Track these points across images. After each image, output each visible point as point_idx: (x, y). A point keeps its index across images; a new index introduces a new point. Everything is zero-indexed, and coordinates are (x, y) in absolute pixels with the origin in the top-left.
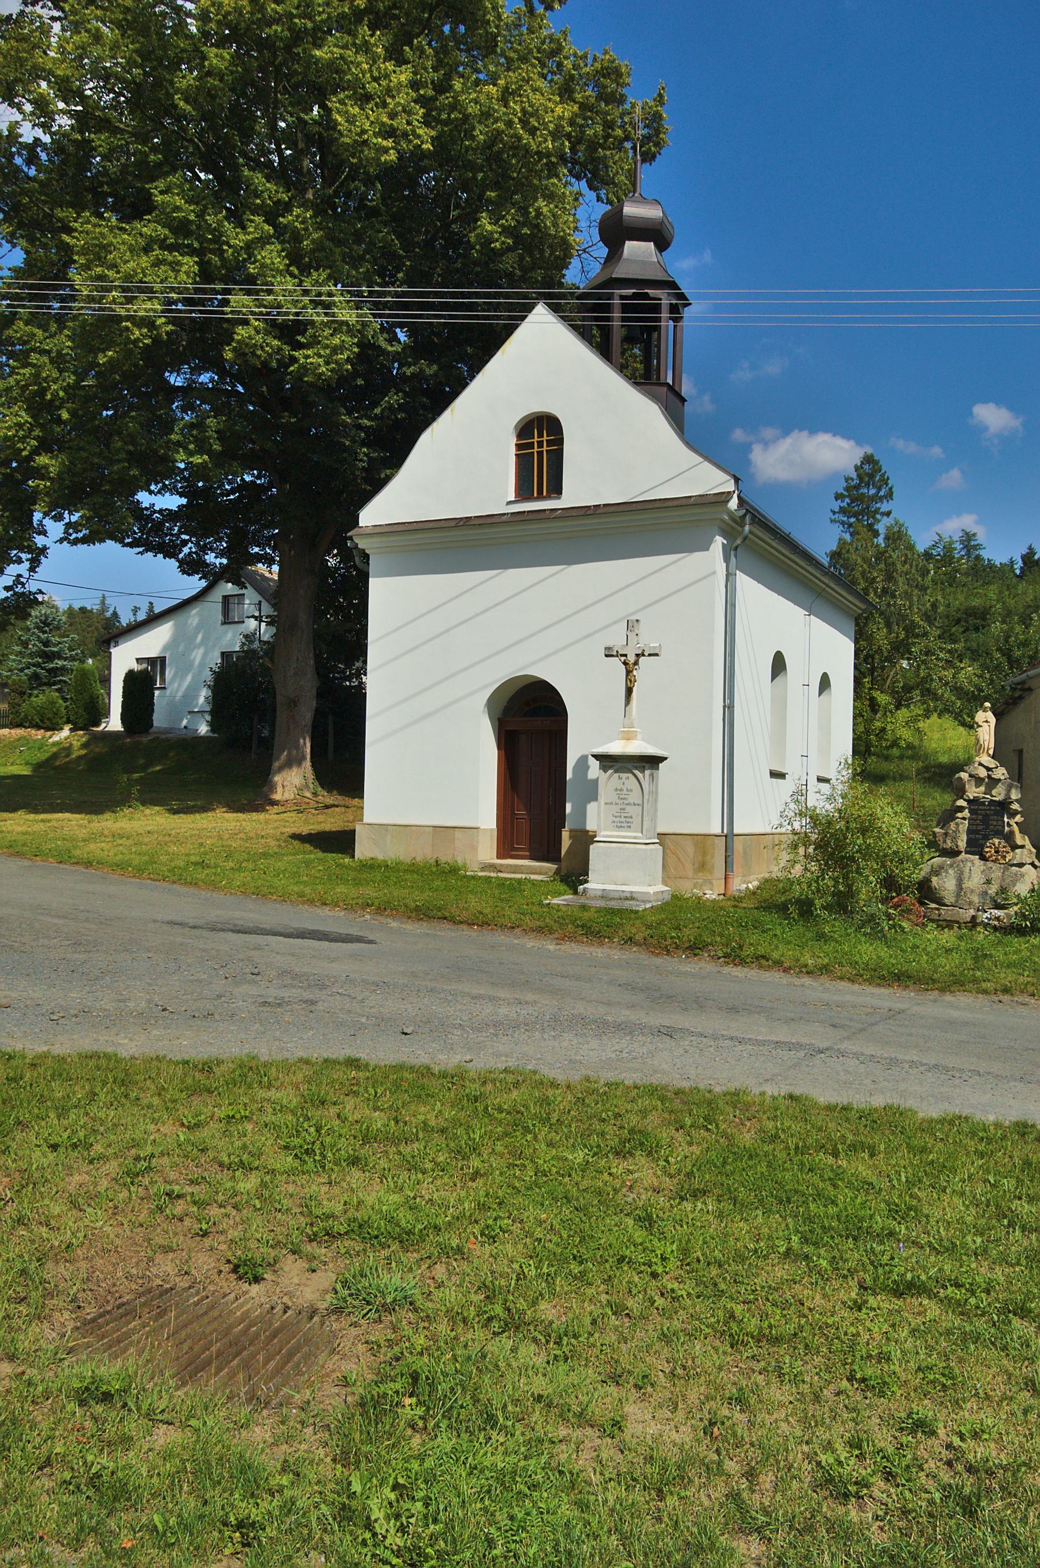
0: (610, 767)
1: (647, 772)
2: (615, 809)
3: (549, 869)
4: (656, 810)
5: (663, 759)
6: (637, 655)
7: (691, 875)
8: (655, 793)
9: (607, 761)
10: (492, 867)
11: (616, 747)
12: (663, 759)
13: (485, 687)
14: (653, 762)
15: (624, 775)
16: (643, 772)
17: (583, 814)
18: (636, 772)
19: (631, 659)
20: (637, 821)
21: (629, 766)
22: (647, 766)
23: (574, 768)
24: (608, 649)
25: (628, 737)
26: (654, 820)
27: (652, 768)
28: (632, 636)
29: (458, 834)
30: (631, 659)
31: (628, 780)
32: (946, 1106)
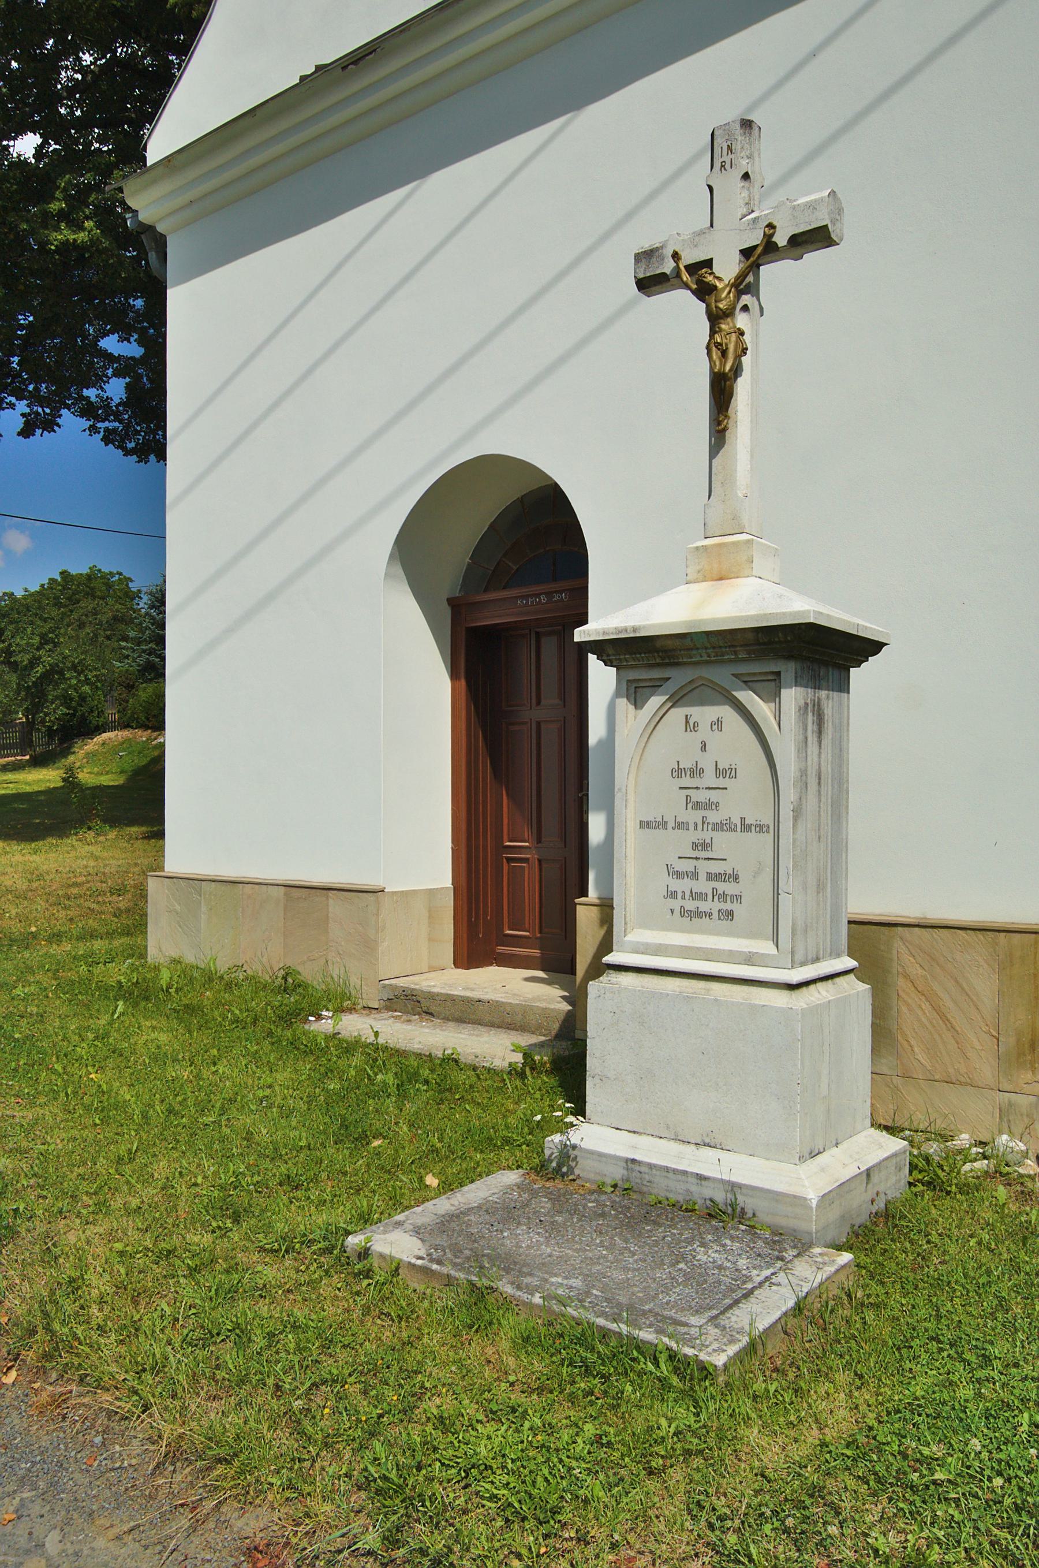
0: (655, 686)
1: (792, 696)
4: (838, 849)
5: (871, 647)
7: (986, 1070)
8: (831, 787)
10: (410, 1003)
12: (871, 647)
13: (384, 504)
14: (822, 654)
15: (705, 714)
16: (773, 696)
18: (747, 697)
19: (727, 269)
20: (754, 889)
21: (721, 675)
22: (788, 669)
24: (645, 256)
25: (720, 567)
26: (830, 878)
27: (815, 682)
29: (335, 905)
30: (727, 269)
31: (716, 732)
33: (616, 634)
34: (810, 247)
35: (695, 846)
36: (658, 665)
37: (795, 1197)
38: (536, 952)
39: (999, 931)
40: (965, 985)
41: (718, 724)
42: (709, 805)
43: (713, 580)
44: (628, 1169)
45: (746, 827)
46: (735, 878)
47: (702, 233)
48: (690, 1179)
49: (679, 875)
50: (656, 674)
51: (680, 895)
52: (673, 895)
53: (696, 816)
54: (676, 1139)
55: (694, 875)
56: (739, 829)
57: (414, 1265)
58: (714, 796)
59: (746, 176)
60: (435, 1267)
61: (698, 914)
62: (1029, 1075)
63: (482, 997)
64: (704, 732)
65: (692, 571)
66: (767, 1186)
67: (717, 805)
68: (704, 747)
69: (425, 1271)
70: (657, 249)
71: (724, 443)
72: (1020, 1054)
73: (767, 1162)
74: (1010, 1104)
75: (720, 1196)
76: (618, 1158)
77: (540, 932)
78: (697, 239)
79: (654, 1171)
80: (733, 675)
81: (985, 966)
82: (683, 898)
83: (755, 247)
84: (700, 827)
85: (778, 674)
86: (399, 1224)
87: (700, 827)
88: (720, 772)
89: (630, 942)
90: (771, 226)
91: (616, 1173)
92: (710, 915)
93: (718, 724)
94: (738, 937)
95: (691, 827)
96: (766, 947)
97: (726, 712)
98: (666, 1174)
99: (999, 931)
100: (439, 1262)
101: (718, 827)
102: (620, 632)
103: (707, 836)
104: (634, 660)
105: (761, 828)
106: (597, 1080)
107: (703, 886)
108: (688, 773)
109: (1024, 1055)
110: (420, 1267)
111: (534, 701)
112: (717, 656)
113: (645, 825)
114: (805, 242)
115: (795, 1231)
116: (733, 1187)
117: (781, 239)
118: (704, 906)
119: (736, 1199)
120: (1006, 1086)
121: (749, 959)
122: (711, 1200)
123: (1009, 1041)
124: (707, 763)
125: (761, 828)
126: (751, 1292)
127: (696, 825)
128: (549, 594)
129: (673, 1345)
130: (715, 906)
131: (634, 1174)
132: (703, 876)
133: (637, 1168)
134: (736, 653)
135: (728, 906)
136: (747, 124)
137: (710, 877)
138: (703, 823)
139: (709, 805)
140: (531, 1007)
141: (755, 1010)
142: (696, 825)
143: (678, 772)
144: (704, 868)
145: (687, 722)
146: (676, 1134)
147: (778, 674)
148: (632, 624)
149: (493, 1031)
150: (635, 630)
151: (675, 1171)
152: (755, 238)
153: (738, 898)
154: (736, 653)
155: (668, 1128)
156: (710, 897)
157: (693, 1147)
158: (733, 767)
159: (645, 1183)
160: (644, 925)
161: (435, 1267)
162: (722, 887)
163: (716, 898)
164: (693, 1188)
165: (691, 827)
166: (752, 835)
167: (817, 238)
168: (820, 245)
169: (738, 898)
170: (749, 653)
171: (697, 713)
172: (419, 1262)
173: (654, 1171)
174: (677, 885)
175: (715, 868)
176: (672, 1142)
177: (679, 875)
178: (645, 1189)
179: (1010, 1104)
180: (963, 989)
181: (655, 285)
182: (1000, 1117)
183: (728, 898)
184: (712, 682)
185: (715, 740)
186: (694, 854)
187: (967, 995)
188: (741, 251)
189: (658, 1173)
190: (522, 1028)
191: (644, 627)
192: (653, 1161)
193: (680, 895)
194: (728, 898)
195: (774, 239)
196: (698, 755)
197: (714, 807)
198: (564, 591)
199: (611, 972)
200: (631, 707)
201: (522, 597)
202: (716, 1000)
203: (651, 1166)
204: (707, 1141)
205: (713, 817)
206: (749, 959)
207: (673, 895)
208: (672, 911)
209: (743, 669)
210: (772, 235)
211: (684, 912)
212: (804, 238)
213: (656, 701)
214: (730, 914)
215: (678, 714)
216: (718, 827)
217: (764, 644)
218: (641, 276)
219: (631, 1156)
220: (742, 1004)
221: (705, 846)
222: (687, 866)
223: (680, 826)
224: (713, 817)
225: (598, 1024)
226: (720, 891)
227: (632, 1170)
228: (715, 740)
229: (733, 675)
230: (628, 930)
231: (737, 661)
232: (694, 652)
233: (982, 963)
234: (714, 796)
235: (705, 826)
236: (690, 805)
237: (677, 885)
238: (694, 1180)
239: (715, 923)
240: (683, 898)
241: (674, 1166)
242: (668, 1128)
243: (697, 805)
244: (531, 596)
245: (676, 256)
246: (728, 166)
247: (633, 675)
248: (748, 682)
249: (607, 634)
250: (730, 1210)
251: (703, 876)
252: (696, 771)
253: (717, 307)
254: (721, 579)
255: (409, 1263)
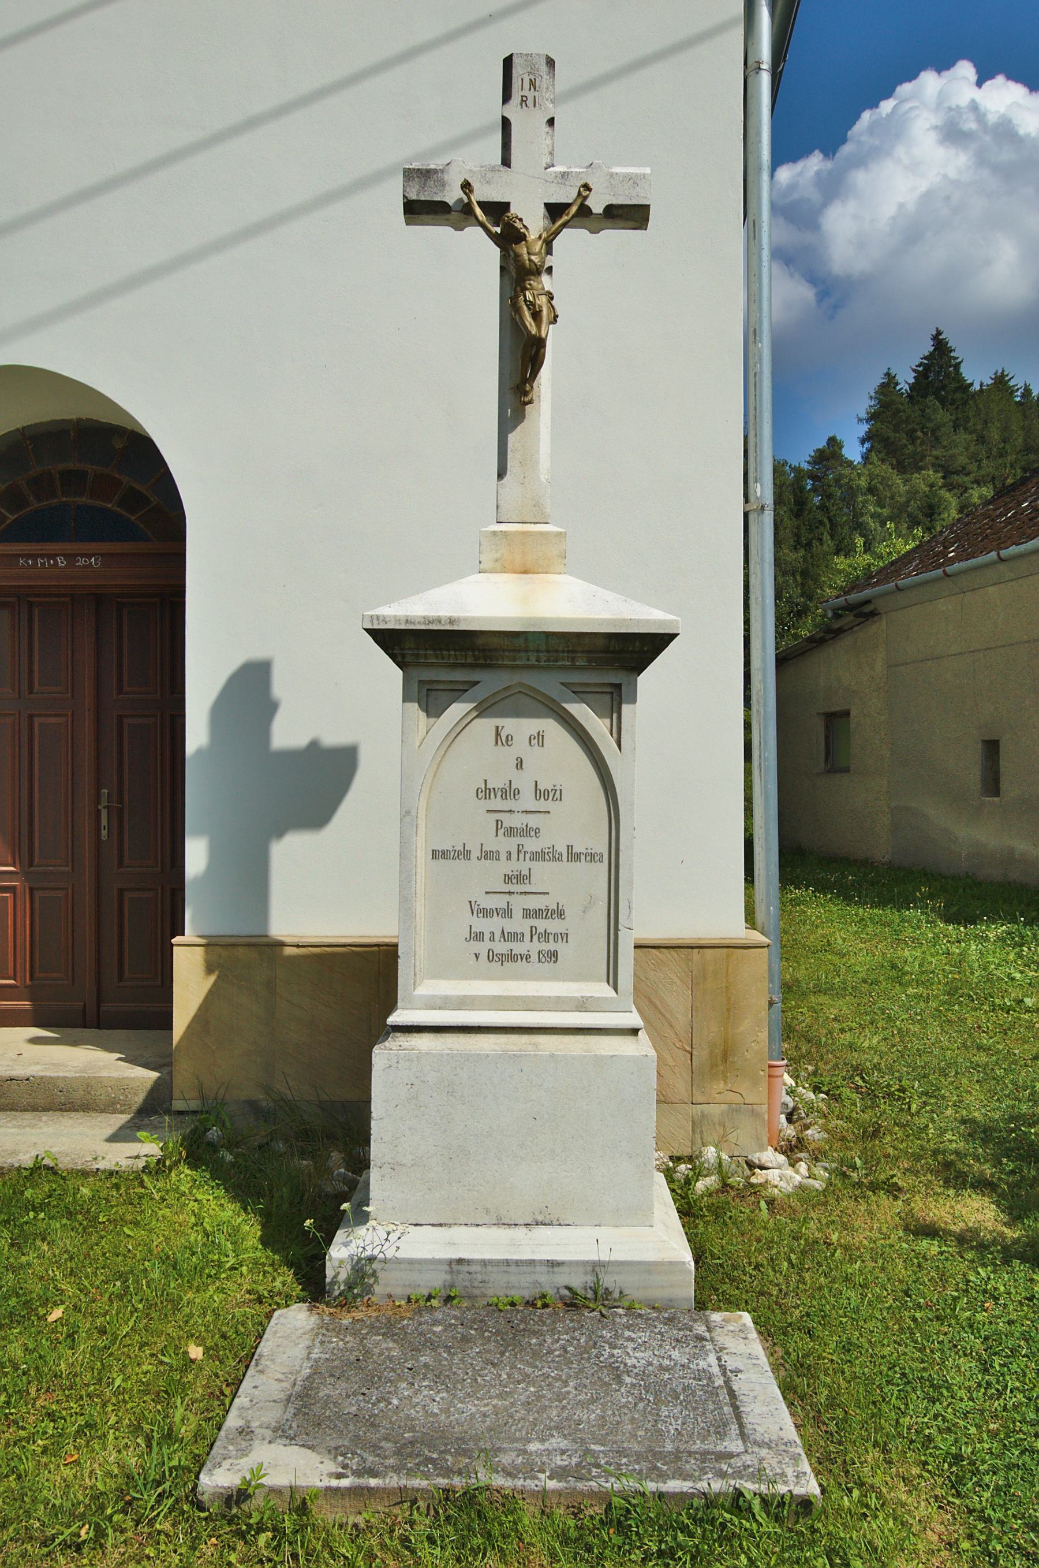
0: (458, 691)
2: (482, 879)
3: (123, 1086)
5: (653, 644)
6: (554, 210)
9: (437, 660)
11: (484, 600)
12: (653, 644)
15: (520, 728)
17: (252, 878)
18: (580, 711)
20: (586, 929)
21: (548, 683)
23: (223, 709)
25: (525, 561)
28: (527, 126)
32: (405, 1044)
33: (425, 623)
34: (622, 223)
35: (508, 879)
36: (463, 666)
37: (671, 1262)
38: (26, 1005)
39: (692, 948)
40: (658, 1003)
41: (539, 738)
42: (526, 831)
43: (515, 572)
44: (451, 1272)
45: (573, 856)
46: (560, 914)
47: (493, 169)
48: (538, 1268)
49: (486, 913)
50: (460, 675)
51: (487, 936)
52: (479, 937)
53: (511, 844)
54: (500, 1223)
55: (508, 912)
56: (565, 858)
57: (337, 1489)
58: (533, 821)
59: (551, 122)
60: (373, 1482)
61: (512, 957)
62: (722, 1085)
63: (14, 1073)
64: (520, 747)
65: (488, 559)
66: (629, 1259)
67: (537, 831)
68: (520, 764)
69: (356, 1492)
70: (435, 171)
71: (524, 417)
72: (713, 1066)
73: (616, 1229)
74: (703, 1115)
75: (578, 1281)
76: (440, 1262)
77: (31, 979)
78: (489, 175)
79: (489, 1268)
80: (562, 684)
81: (679, 983)
82: (492, 939)
83: (568, 206)
84: (514, 856)
85: (619, 687)
86: (245, 1432)
87: (514, 856)
88: (539, 793)
89: (421, 996)
90: (587, 187)
91: (436, 1280)
92: (528, 957)
93: (539, 738)
94: (564, 980)
95: (503, 856)
96: (602, 990)
97: (550, 726)
98: (505, 1268)
99: (692, 948)
100: (373, 1473)
101: (538, 856)
102: (430, 622)
103: (523, 867)
104: (437, 657)
105: (592, 857)
106: (386, 1169)
107: (518, 924)
108: (499, 794)
109: (716, 1065)
110: (349, 1489)
111: (25, 687)
112: (548, 660)
113: (437, 855)
114: (620, 217)
115: (671, 1300)
116: (596, 1267)
117: (597, 204)
118: (518, 948)
119: (598, 1280)
120: (699, 1098)
121: (582, 1005)
122: (569, 1289)
123: (701, 1055)
124: (524, 782)
125: (592, 857)
126: (732, 1393)
127: (509, 854)
128: (71, 557)
129: (763, 1488)
130: (535, 947)
131: (461, 1276)
132: (518, 913)
133: (465, 1268)
134: (573, 660)
135: (551, 946)
136: (551, 63)
137: (527, 914)
138: (519, 851)
139: (526, 831)
140: (99, 1080)
141: (599, 1061)
142: (509, 854)
143: (486, 792)
144: (519, 904)
145: (498, 734)
146: (499, 1218)
147: (619, 687)
148: (448, 614)
149: (45, 1117)
150: (451, 621)
151: (518, 1263)
152: (566, 195)
153: (564, 937)
154: (573, 660)
155: (488, 1211)
156: (527, 937)
157: (523, 1230)
158: (558, 788)
159: (476, 1284)
160: (437, 973)
161: (373, 1482)
162: (542, 925)
163: (535, 938)
164: (543, 1279)
165: (503, 856)
166: (583, 865)
167: (632, 216)
168: (632, 224)
169: (564, 937)
170: (589, 660)
171: (509, 725)
172: (345, 1483)
173: (489, 1268)
174: (482, 925)
175: (534, 903)
176: (494, 1229)
177: (486, 913)
178: (477, 1292)
179: (703, 1115)
180: (656, 1007)
181: (428, 213)
182: (693, 1131)
183: (551, 937)
184: (534, 690)
185: (533, 756)
186: (506, 888)
187: (660, 1012)
188: (545, 204)
189: (495, 1269)
190: (109, 1107)
191: (465, 619)
192: (487, 1256)
193: (487, 936)
194: (551, 937)
195: (587, 203)
196: (512, 773)
197: (533, 833)
198: (94, 555)
199: (399, 1035)
200: (422, 715)
201: (28, 556)
202: (552, 1056)
203: (484, 1263)
204: (540, 1218)
205: (532, 845)
206: (582, 1005)
207: (479, 937)
208: (477, 956)
209: (576, 678)
210: (586, 198)
211: (491, 956)
212: (620, 212)
213: (458, 710)
214: (554, 956)
215: (486, 726)
216: (538, 856)
217: (613, 652)
218: (413, 196)
219: (456, 1256)
220: (585, 1056)
221: (521, 878)
222: (499, 902)
223: (487, 855)
224: (532, 845)
225: (387, 1101)
226: (541, 930)
227: (458, 1272)
228: (533, 756)
229: (562, 684)
230: (418, 982)
231: (574, 668)
232: (523, 654)
233: (676, 980)
234: (533, 821)
235: (522, 855)
236: (501, 832)
237: (482, 925)
238: (544, 1269)
239: (535, 966)
240: (492, 939)
241: (515, 1257)
242: (488, 1211)
243: (511, 832)
244: (42, 556)
245: (466, 186)
246: (530, 102)
247: (428, 675)
248: (580, 693)
249: (430, 622)
250: (590, 1294)
251: (518, 913)
252: (510, 792)
253: (530, 260)
254: (525, 572)
255: (328, 1489)
